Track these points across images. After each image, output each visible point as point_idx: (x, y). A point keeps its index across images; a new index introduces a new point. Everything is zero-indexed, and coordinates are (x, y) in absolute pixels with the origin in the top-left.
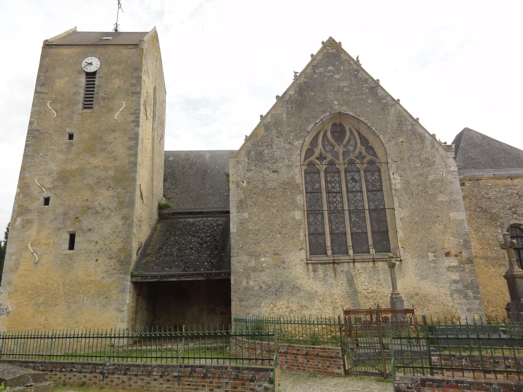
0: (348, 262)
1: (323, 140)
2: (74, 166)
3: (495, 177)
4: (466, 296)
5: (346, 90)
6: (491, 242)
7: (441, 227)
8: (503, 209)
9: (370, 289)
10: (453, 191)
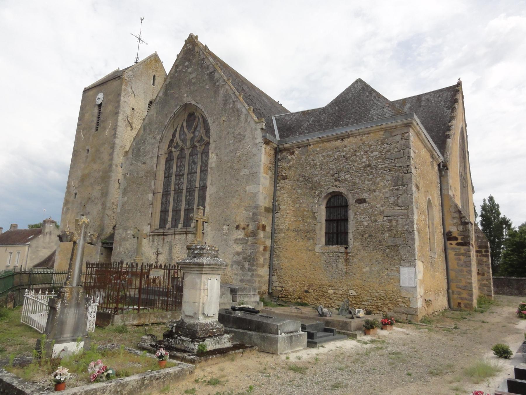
0: (172, 234)
1: (180, 131)
2: (87, 172)
3: (322, 141)
4: (242, 268)
5: (194, 81)
6: (306, 213)
7: (237, 201)
8: (325, 176)
9: (180, 257)
10: (254, 163)
